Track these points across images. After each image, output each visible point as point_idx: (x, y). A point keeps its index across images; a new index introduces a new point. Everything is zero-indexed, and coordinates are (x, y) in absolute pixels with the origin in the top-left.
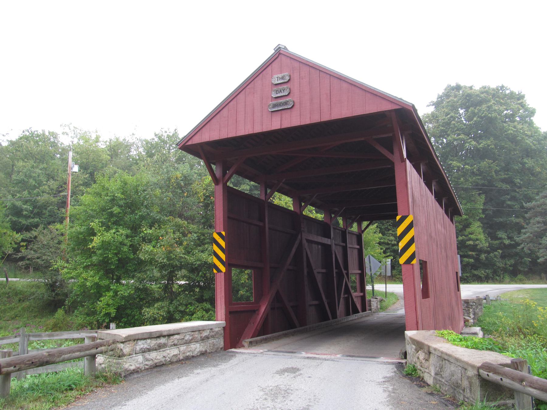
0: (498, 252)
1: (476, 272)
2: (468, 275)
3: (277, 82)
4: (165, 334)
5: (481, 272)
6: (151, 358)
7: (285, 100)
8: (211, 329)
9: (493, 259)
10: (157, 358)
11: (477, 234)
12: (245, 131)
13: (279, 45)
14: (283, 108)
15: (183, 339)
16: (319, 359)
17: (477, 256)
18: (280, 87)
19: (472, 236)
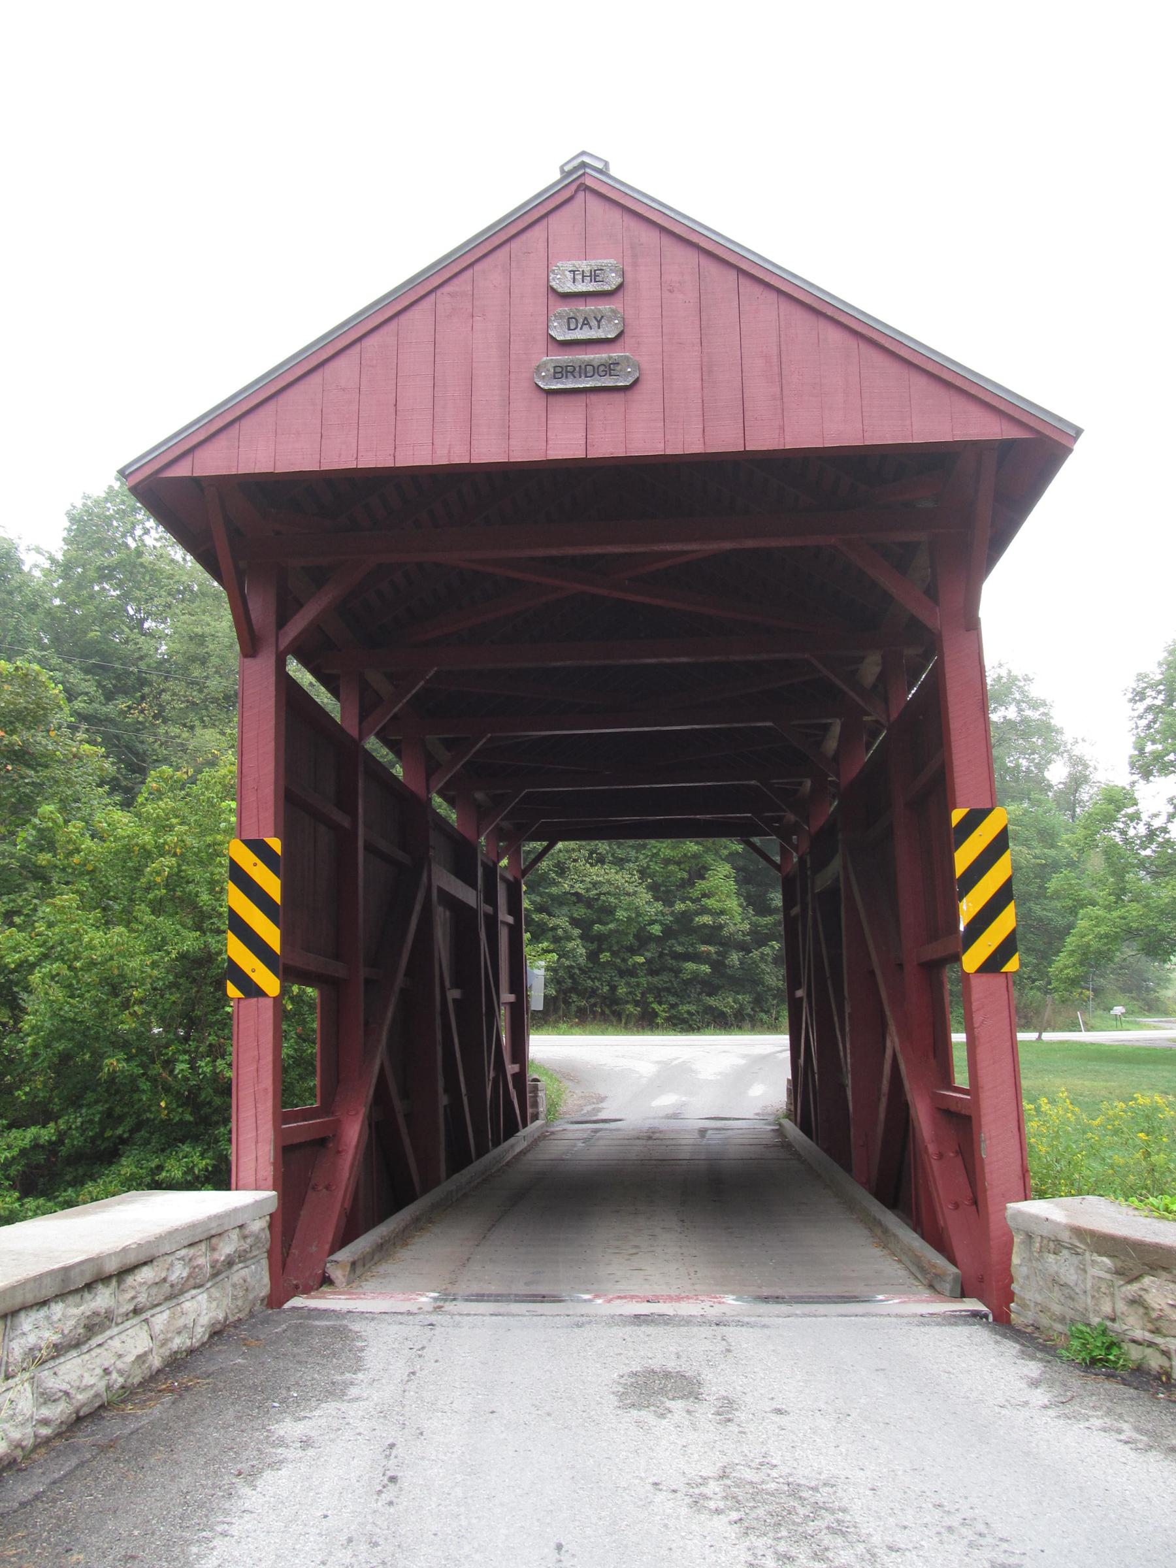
0: (772, 947)
1: (712, 1001)
2: (692, 1008)
3: (569, 287)
4: (112, 1267)
5: (726, 1002)
6: (65, 1387)
7: (604, 356)
8: (241, 1227)
9: (757, 965)
10: (85, 1382)
11: (724, 898)
12: (433, 451)
13: (583, 153)
14: (599, 384)
15: (165, 1280)
16: (687, 1321)
17: (720, 958)
18: (590, 307)
19: (710, 902)
